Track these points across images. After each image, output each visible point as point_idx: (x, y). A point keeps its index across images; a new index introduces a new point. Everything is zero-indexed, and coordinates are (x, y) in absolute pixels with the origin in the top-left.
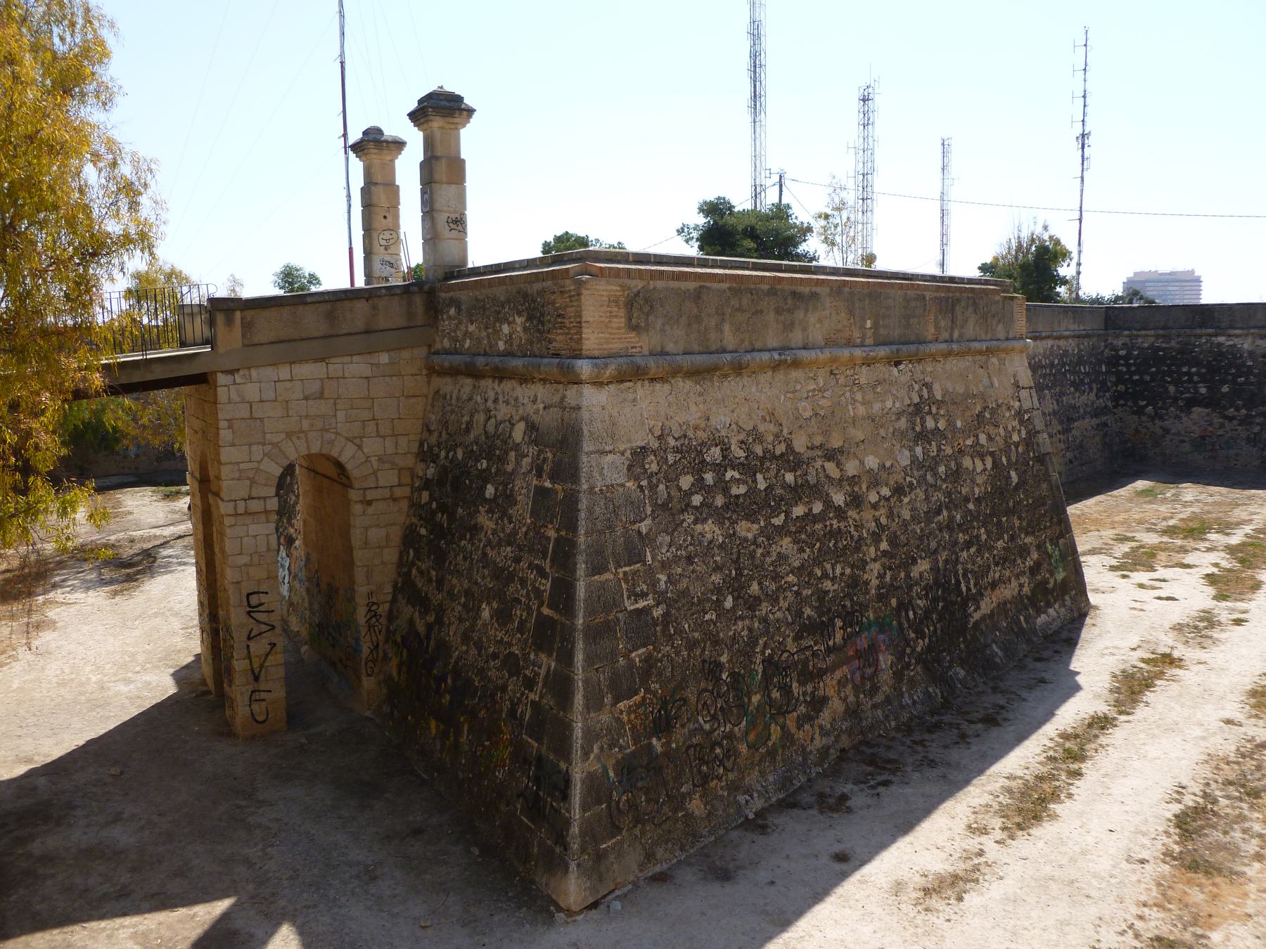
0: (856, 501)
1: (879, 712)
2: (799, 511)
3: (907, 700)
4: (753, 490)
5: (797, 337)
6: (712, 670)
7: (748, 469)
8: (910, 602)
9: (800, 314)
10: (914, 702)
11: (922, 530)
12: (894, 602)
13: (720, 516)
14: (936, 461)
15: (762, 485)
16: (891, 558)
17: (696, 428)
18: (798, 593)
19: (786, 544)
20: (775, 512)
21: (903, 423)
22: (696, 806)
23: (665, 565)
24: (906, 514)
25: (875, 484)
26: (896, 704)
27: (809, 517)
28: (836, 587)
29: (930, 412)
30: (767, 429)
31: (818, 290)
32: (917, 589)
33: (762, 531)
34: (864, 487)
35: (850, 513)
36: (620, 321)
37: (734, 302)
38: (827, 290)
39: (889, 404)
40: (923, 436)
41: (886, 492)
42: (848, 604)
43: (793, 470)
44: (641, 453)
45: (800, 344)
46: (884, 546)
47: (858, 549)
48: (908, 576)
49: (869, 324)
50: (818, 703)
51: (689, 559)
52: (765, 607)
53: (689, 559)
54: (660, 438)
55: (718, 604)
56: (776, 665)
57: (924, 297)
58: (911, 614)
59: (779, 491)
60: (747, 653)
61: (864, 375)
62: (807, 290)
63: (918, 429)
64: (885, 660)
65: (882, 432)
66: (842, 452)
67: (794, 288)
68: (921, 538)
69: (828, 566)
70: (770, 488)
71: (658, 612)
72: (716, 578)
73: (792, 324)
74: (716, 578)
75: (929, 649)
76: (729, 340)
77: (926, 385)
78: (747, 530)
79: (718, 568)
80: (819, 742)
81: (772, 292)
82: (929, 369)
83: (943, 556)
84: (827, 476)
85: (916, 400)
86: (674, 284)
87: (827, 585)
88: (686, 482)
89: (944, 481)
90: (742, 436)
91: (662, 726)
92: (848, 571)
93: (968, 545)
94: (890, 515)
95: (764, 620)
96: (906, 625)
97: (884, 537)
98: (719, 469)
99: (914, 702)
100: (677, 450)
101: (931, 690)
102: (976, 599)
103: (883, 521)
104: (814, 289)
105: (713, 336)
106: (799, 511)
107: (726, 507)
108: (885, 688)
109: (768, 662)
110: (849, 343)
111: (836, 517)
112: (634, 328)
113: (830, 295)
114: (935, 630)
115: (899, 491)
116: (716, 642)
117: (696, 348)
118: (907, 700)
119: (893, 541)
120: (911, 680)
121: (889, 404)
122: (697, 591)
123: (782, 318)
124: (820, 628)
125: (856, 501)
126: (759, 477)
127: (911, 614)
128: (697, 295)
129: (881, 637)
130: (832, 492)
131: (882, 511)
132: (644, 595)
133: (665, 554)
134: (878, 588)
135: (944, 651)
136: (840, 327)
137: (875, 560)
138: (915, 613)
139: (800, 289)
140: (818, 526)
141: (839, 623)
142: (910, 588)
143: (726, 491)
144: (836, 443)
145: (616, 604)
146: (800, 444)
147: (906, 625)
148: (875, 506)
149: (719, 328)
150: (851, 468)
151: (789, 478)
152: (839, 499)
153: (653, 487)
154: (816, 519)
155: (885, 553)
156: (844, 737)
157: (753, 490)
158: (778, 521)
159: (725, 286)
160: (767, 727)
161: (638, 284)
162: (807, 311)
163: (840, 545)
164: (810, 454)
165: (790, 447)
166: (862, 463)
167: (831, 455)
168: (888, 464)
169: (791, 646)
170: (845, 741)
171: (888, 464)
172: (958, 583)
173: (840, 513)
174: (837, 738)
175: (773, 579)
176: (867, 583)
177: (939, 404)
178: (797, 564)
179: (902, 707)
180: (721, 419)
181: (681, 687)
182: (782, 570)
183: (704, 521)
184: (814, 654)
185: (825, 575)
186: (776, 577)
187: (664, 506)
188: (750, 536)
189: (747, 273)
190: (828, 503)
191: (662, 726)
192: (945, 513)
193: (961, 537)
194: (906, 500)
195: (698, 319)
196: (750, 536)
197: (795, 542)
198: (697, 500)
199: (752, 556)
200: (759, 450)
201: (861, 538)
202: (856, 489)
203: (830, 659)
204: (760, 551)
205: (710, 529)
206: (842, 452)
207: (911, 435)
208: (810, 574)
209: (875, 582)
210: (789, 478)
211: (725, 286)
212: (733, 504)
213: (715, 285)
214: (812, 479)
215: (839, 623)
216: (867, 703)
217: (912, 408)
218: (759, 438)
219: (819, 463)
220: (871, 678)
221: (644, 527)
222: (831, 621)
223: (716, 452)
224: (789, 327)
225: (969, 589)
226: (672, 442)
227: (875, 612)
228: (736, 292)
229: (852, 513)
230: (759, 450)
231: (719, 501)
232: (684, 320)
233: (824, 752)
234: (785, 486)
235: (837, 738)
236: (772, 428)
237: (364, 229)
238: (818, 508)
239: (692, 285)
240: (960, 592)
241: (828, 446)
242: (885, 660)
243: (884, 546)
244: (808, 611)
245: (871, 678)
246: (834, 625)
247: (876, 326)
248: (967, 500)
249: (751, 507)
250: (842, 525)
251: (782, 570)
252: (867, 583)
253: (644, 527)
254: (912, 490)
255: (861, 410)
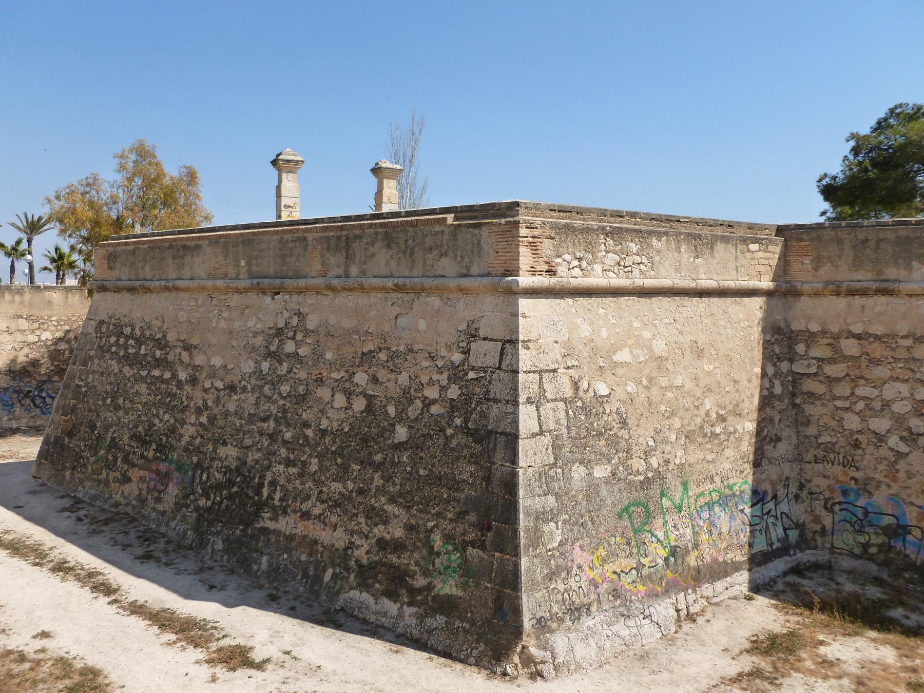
0: (193, 381)
1: (154, 514)
2: (156, 373)
3: (173, 524)
4: (137, 353)
5: (187, 273)
6: (93, 427)
7: (139, 342)
8: (208, 468)
9: (188, 259)
10: (175, 529)
11: (241, 425)
12: (195, 459)
13: (119, 359)
14: (281, 379)
15: (143, 352)
16: (206, 430)
17: (125, 316)
18: (139, 416)
19: (143, 388)
20: (143, 368)
21: (259, 341)
22: (68, 474)
23: (94, 372)
24: (231, 407)
25: (212, 376)
26: (166, 519)
27: (161, 379)
28: (161, 425)
29: (293, 338)
30: (156, 323)
31: (200, 242)
32: (216, 464)
33: (134, 375)
34: (204, 375)
35: (186, 387)
36: (106, 266)
37: (151, 254)
38: (207, 242)
39: (251, 324)
40: (276, 356)
41: (219, 384)
42: (164, 439)
43: (161, 349)
44: (102, 322)
45: (189, 277)
46: (204, 419)
47: (183, 411)
48: (215, 450)
49: (243, 263)
50: (126, 479)
51: (102, 374)
52: (121, 413)
53: (102, 374)
54: (110, 317)
55: (104, 400)
56: (116, 444)
57: (305, 239)
58: (205, 476)
59: (149, 358)
60: (107, 428)
61: (235, 300)
62: (192, 244)
63: (273, 349)
64: (173, 491)
65: (234, 343)
66: (196, 348)
67: (184, 243)
68: (238, 431)
69: (161, 412)
70: (145, 355)
71: (84, 389)
72: (109, 388)
73: (183, 265)
74: (109, 388)
75: (209, 510)
76: (148, 273)
77: (299, 314)
78: (128, 371)
79: (110, 383)
80: (118, 498)
81: (171, 247)
82: (309, 302)
83: (253, 456)
84: (180, 359)
85: (281, 324)
86: (125, 248)
87: (156, 421)
88: (113, 340)
89: (284, 398)
90: (142, 324)
91: (71, 435)
92: (172, 421)
93: (289, 463)
94: (217, 401)
95: (119, 419)
96: (197, 480)
97: (205, 413)
98: (127, 337)
99: (175, 529)
100: (114, 325)
101: (189, 532)
102: (281, 511)
103: (210, 403)
104: (198, 243)
105: (140, 271)
106: (156, 373)
107: (124, 356)
108: (166, 505)
109: (113, 439)
110: (225, 277)
111: (176, 386)
112: (110, 268)
113: (210, 245)
114: (221, 503)
115: (232, 388)
116: (98, 416)
117: (133, 277)
118: (173, 524)
119: (212, 419)
120: (184, 516)
121: (251, 324)
122: (99, 388)
123: (176, 261)
124: (143, 441)
125: (193, 381)
126: (143, 347)
127: (205, 476)
128: (134, 253)
129: (176, 474)
130: (180, 369)
131: (210, 396)
132: (82, 380)
133: (95, 367)
134: (188, 443)
135: (221, 522)
136: (218, 266)
137: (192, 425)
138: (208, 477)
139: (189, 243)
140: (164, 386)
141: (154, 446)
142: (212, 459)
143: (126, 349)
144: (194, 341)
145: (74, 378)
146: (171, 337)
147: (197, 480)
148: (206, 391)
149: (143, 268)
150: (199, 360)
151: (158, 353)
152: (183, 376)
153: (101, 338)
154: (163, 381)
155: (201, 424)
156: (130, 508)
157: (137, 353)
158: (144, 373)
159: (146, 246)
160: (101, 468)
161: (111, 249)
162: (192, 256)
163: (172, 403)
164: (175, 343)
165: (164, 336)
166: (209, 360)
167: (187, 348)
168: (230, 367)
169: (126, 439)
170: (129, 509)
171: (230, 367)
172: (261, 485)
173: (180, 384)
174: (127, 504)
175: (130, 401)
176: (181, 436)
177: (307, 333)
178: (144, 400)
179: (167, 525)
180: (137, 314)
181: (80, 424)
182: (136, 399)
183: (113, 360)
184: (134, 453)
185: (157, 415)
186: (132, 401)
187: (101, 347)
188: (128, 375)
189: (414, 218)
190: (174, 376)
191: (71, 435)
192: (272, 424)
193: (283, 452)
194: (235, 397)
195: (134, 264)
196: (128, 375)
197: (149, 389)
198: (114, 349)
199: (125, 385)
200: (148, 333)
201: (187, 406)
202: (197, 374)
203: (141, 462)
204: (129, 384)
205: (114, 366)
206: (196, 348)
207: (263, 351)
208: (149, 410)
209: (186, 439)
210: (158, 353)
211: (146, 246)
212: (127, 356)
213: (142, 246)
214: (170, 358)
215: (154, 446)
216: (151, 503)
217: (273, 331)
218: (149, 328)
219: (178, 350)
220: (160, 492)
221: (92, 353)
222: (150, 442)
223: (129, 329)
224: (181, 267)
225: (270, 497)
226: (113, 321)
227: (179, 456)
228: (151, 249)
229: (188, 388)
230: (148, 333)
231: (122, 353)
232: (128, 264)
233: (117, 504)
234: (154, 356)
235: (127, 504)
236: (159, 324)
237: (482, 206)
238: (167, 375)
239: (131, 247)
240: (259, 494)
241: (189, 342)
242: (173, 491)
243: (204, 419)
244: (140, 429)
245: (160, 492)
246: (151, 446)
247: (249, 264)
248: (306, 425)
249: (129, 360)
250: (178, 391)
251: (136, 399)
252: (181, 436)
253: (92, 353)
254: (244, 392)
255: (223, 324)
